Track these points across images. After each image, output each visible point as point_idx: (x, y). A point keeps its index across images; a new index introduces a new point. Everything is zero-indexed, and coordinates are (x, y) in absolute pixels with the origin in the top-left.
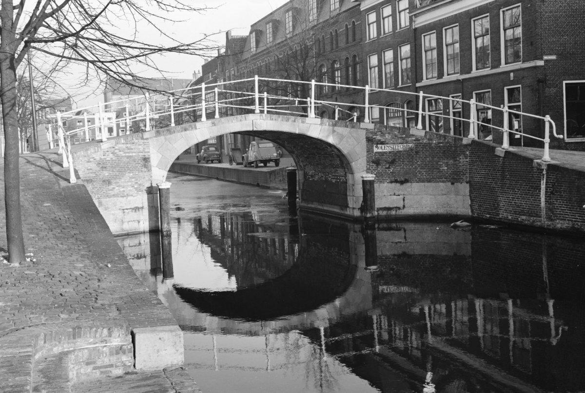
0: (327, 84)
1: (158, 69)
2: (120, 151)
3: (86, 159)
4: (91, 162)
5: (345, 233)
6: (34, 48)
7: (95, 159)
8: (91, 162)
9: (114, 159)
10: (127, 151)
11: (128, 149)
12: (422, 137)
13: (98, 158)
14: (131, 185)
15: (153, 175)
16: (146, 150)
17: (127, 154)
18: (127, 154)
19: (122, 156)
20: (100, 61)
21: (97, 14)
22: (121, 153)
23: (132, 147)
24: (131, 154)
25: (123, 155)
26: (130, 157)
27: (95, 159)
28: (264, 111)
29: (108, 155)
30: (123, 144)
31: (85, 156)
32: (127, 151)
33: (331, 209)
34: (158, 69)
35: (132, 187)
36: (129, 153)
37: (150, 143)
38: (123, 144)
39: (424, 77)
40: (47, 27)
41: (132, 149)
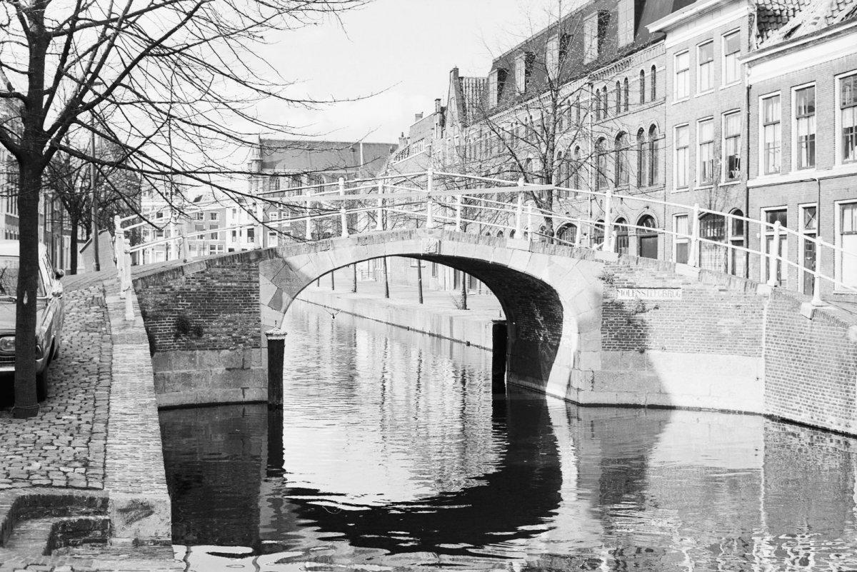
0: (564, 189)
1: (131, 103)
2: (213, 279)
3: (159, 288)
4: (166, 293)
5: (728, 41)
6: (69, 67)
7: (172, 290)
8: (166, 293)
9: (202, 290)
10: (223, 278)
11: (226, 276)
12: (597, 82)
13: (177, 288)
14: (226, 332)
15: (262, 318)
16: (254, 279)
17: (224, 284)
18: (224, 284)
19: (215, 287)
20: (141, 102)
21: (192, 10)
22: (214, 281)
23: (233, 273)
24: (229, 284)
25: (217, 285)
26: (229, 288)
27: (172, 290)
28: (219, 249)
29: (193, 284)
30: (218, 267)
31: (158, 285)
32: (223, 278)
33: (647, 175)
34: (131, 103)
35: (229, 335)
36: (226, 282)
37: (261, 268)
38: (218, 267)
39: (762, 172)
40: (90, 26)
41: (232, 276)
